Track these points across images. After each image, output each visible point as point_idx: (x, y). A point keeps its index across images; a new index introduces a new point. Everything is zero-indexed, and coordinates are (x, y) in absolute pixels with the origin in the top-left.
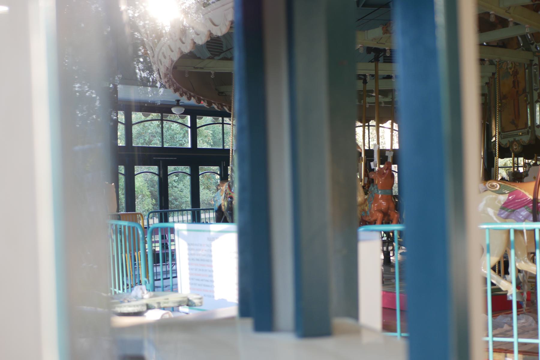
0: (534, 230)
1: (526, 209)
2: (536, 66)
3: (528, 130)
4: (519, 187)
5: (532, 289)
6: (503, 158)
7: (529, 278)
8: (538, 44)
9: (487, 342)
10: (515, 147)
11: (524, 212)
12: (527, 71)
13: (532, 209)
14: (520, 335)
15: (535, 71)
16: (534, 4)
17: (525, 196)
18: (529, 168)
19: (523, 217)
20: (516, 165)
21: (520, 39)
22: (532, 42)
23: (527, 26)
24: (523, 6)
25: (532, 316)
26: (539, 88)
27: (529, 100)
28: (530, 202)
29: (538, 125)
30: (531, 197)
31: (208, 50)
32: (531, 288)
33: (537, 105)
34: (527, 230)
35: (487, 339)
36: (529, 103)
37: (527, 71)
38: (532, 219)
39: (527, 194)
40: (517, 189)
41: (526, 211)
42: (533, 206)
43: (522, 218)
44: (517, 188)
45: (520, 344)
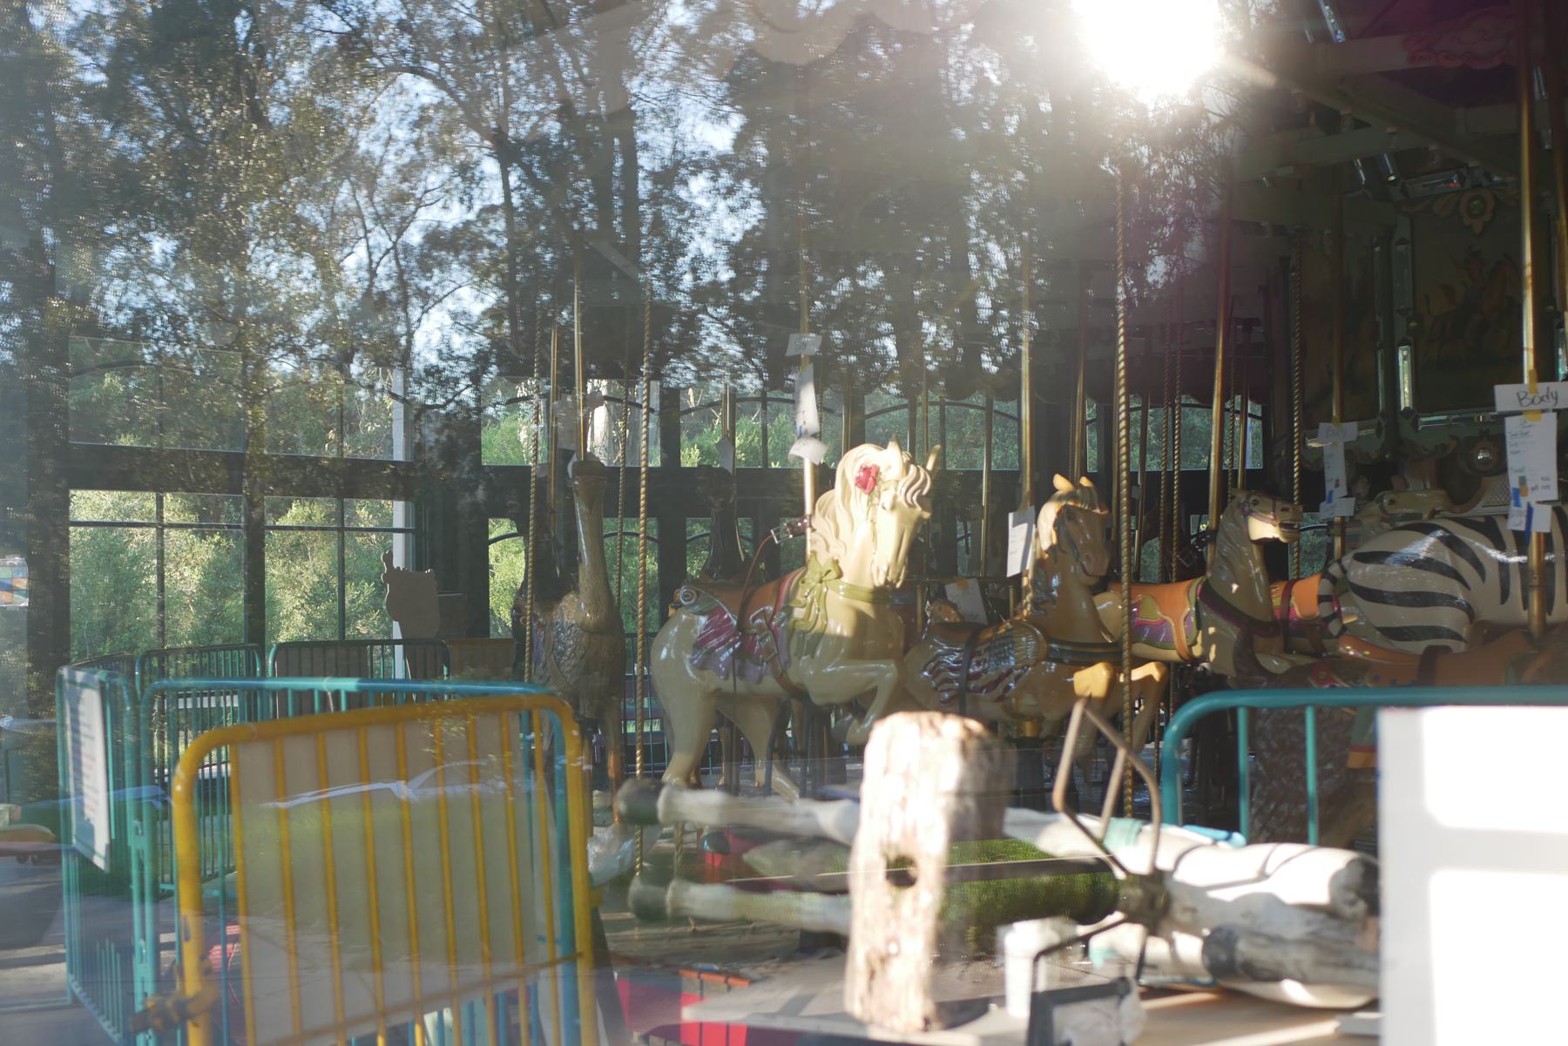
3: (1379, 423)
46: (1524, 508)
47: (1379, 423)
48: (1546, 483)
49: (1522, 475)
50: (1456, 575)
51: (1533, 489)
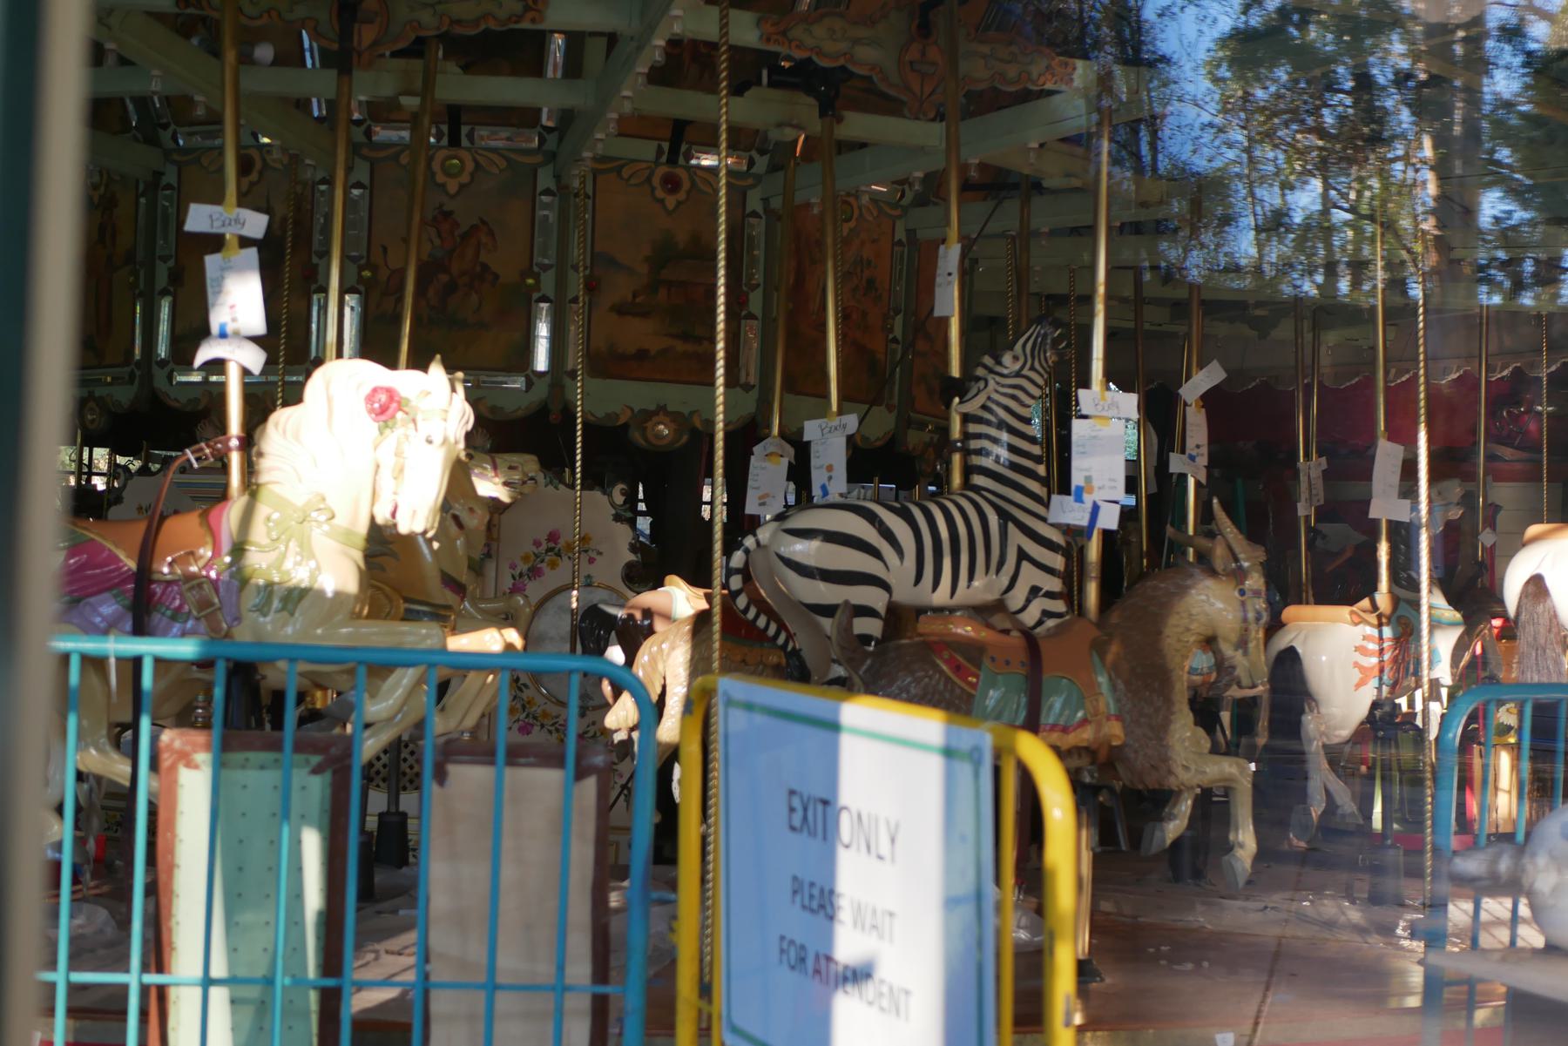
0: (137, 661)
1: (115, 596)
2: (168, 192)
3: (132, 372)
4: (98, 534)
5: (108, 829)
6: (1450, 604)
7: (105, 798)
8: (178, 129)
9: (52, 986)
10: (89, 417)
11: (108, 607)
12: (143, 200)
13: (131, 598)
14: (75, 963)
15: (167, 204)
16: (178, 15)
17: (117, 559)
18: (126, 480)
19: (104, 619)
20: (86, 470)
21: (131, 107)
22: (165, 121)
23: (156, 72)
24: (149, 14)
25: (106, 907)
26: (171, 256)
27: (142, 286)
28: (129, 576)
29: (162, 360)
30: (131, 564)
31: (1186, 381)
32: (106, 826)
33: (163, 302)
34: (119, 660)
35: (48, 976)
36: (141, 295)
37: (143, 200)
38: (128, 626)
39: (122, 556)
40: (93, 540)
41: (113, 605)
42: (135, 589)
43: (101, 622)
44: (92, 536)
45: (74, 989)
46: (1088, 506)
47: (132, 372)
48: (1113, 484)
49: (1087, 474)
50: (875, 553)
51: (1100, 488)
